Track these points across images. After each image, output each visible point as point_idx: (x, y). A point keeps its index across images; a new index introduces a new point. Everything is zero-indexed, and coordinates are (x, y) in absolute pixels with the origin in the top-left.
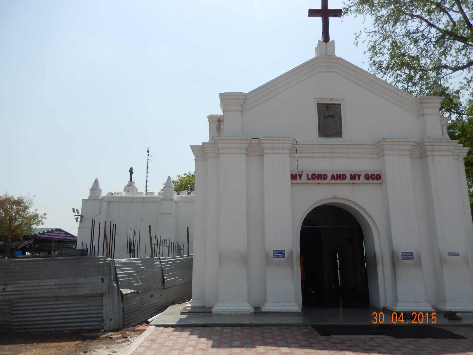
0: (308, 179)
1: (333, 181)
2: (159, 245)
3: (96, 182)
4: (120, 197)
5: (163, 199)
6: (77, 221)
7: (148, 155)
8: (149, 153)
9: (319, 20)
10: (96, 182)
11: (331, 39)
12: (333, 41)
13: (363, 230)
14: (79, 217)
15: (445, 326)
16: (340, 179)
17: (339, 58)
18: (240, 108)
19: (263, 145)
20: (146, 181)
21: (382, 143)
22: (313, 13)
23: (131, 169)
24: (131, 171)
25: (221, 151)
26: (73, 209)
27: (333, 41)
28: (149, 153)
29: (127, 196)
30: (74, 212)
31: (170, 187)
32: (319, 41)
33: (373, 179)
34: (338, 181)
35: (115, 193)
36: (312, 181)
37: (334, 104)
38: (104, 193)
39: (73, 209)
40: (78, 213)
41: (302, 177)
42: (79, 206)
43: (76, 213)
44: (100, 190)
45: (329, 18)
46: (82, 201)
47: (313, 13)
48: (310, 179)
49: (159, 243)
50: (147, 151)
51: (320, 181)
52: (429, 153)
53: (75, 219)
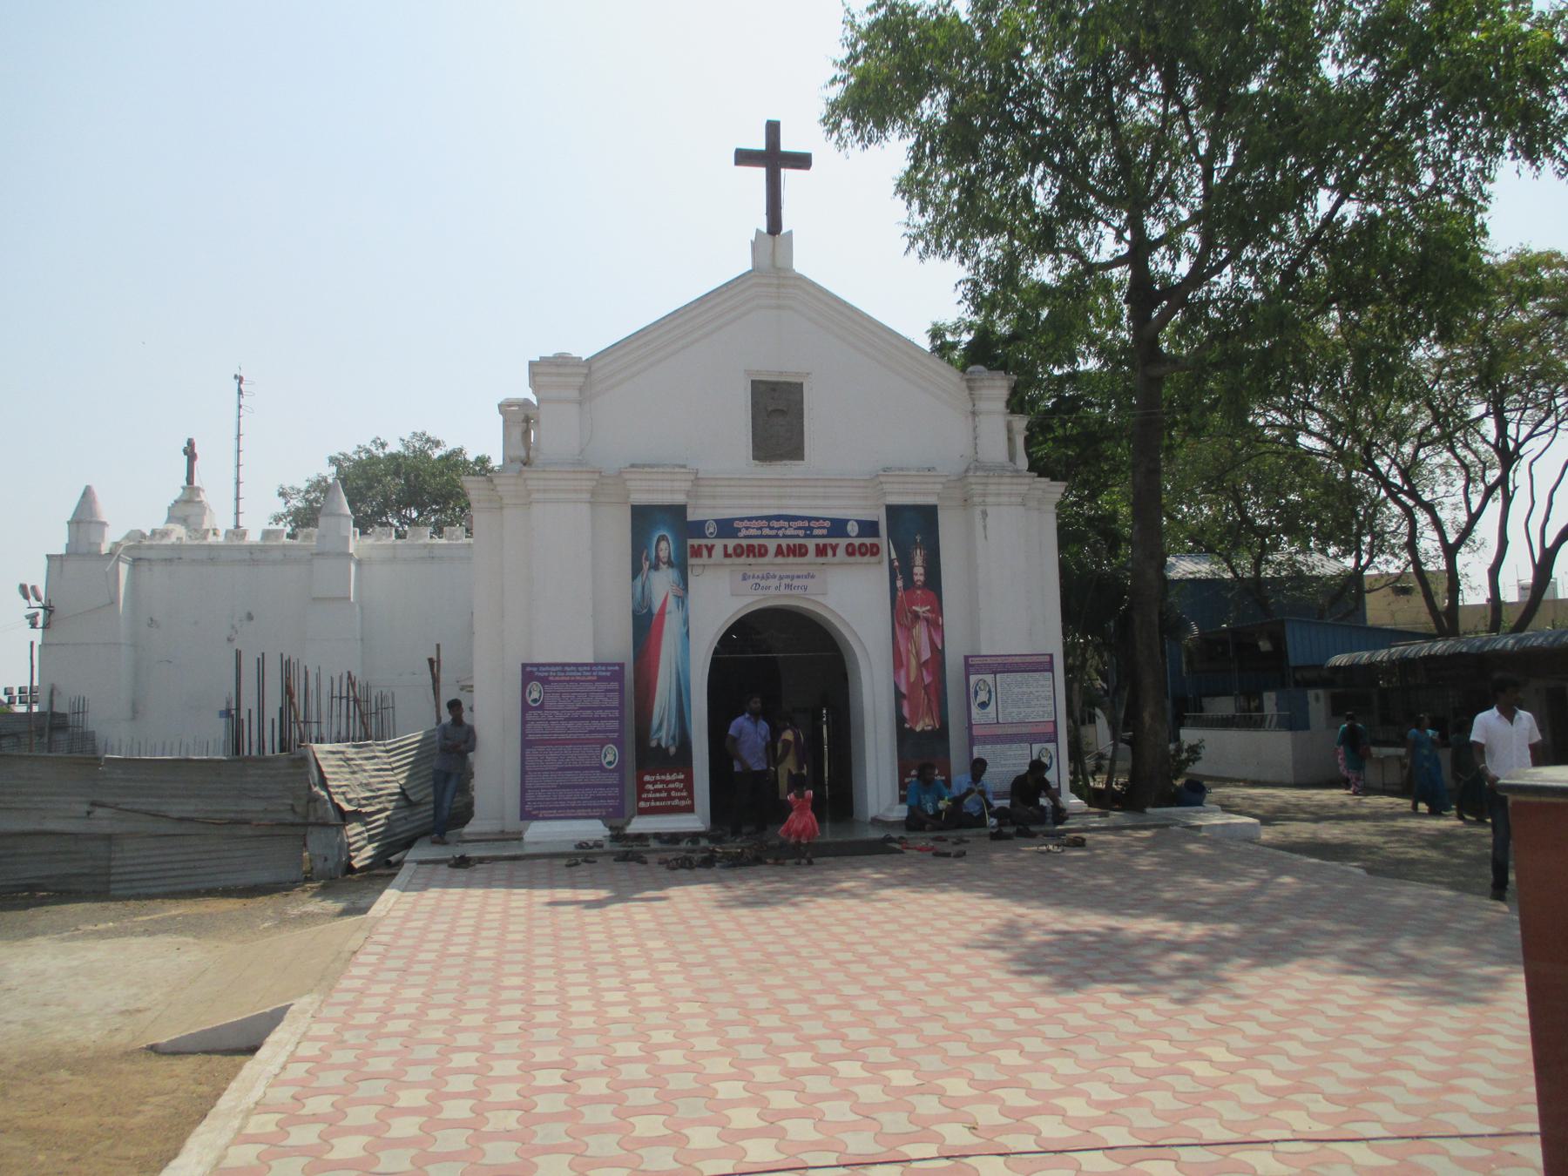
0: (726, 555)
1: (780, 560)
2: (336, 693)
3: (87, 494)
4: (173, 547)
5: (317, 554)
6: (34, 626)
7: (240, 392)
8: (240, 382)
9: (759, 174)
10: (87, 494)
11: (785, 230)
12: (790, 233)
13: (846, 658)
14: (41, 611)
15: (1475, 967)
16: (795, 555)
17: (801, 278)
18: (574, 394)
19: (628, 483)
20: (234, 481)
21: (882, 479)
22: (744, 157)
23: (191, 443)
24: (190, 453)
25: (535, 496)
26: (23, 588)
27: (790, 233)
28: (240, 382)
29: (196, 542)
30: (26, 597)
31: (340, 515)
32: (758, 232)
33: (863, 554)
34: (791, 559)
35: (154, 532)
36: (735, 560)
37: (789, 384)
38: (113, 535)
39: (23, 588)
40: (38, 599)
41: (714, 553)
42: (38, 579)
43: (32, 599)
44: (104, 524)
45: (782, 170)
46: (45, 561)
47: (744, 157)
48: (730, 556)
49: (344, 694)
50: (236, 377)
51: (751, 560)
52: (977, 500)
53: (27, 617)
